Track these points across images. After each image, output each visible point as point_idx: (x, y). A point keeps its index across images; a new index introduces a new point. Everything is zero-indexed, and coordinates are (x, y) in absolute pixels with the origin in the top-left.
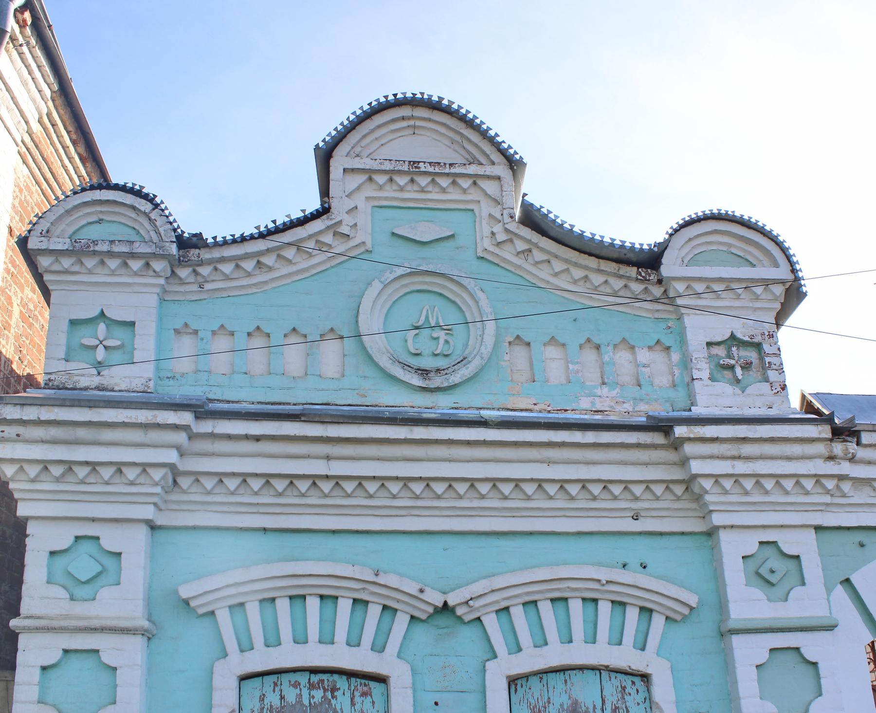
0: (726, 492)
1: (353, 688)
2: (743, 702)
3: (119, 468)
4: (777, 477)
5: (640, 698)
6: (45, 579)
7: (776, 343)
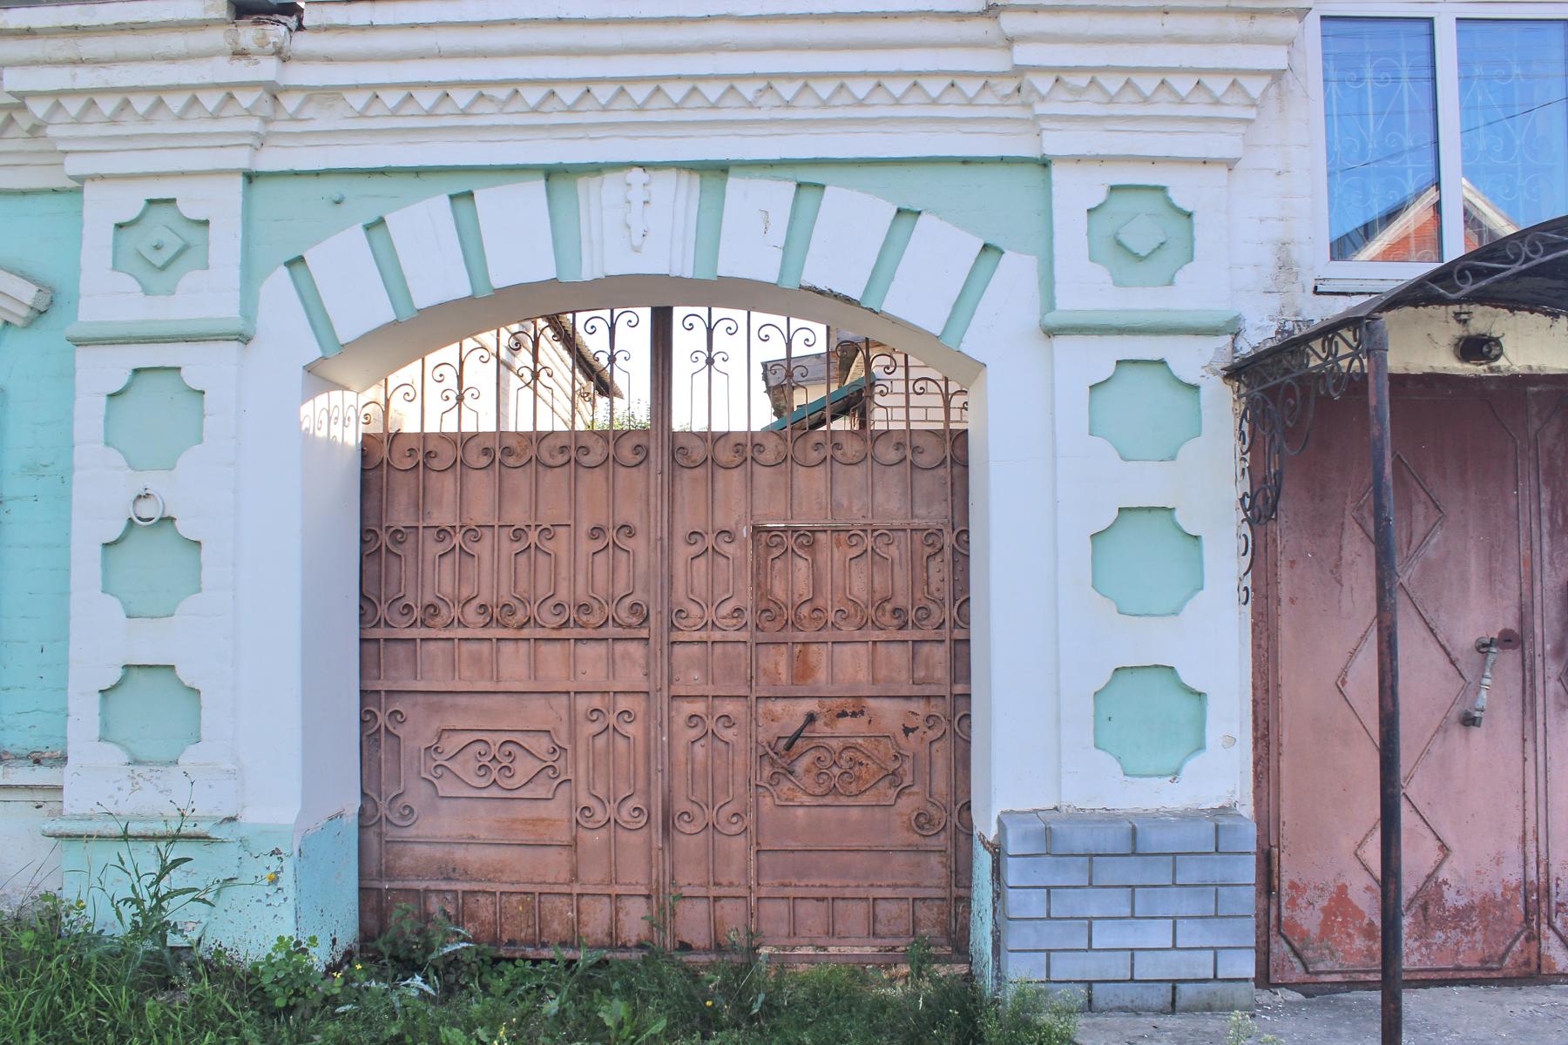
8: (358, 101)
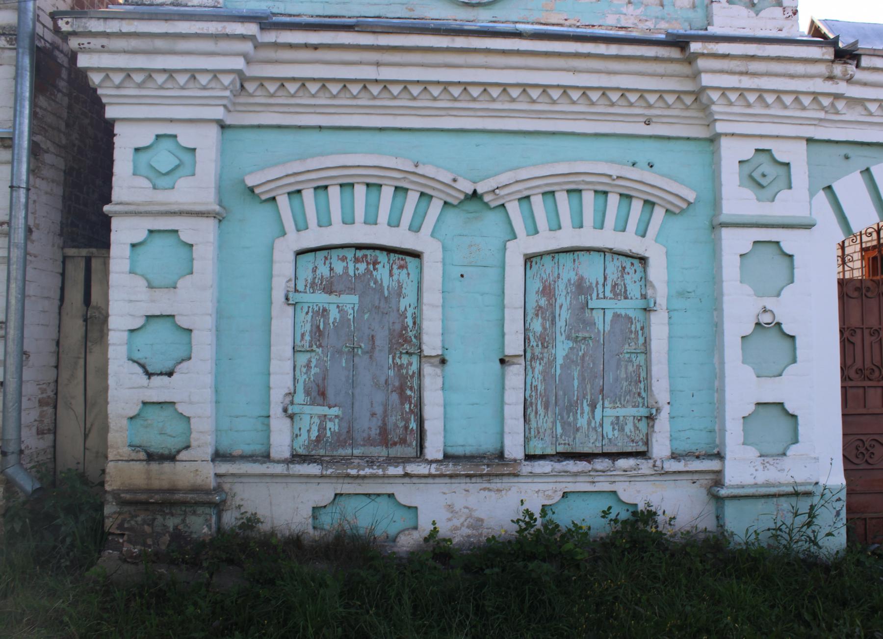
0: (731, 104)
1: (391, 262)
2: (725, 284)
3: (193, 74)
4: (778, 92)
5: (637, 277)
6: (131, 171)
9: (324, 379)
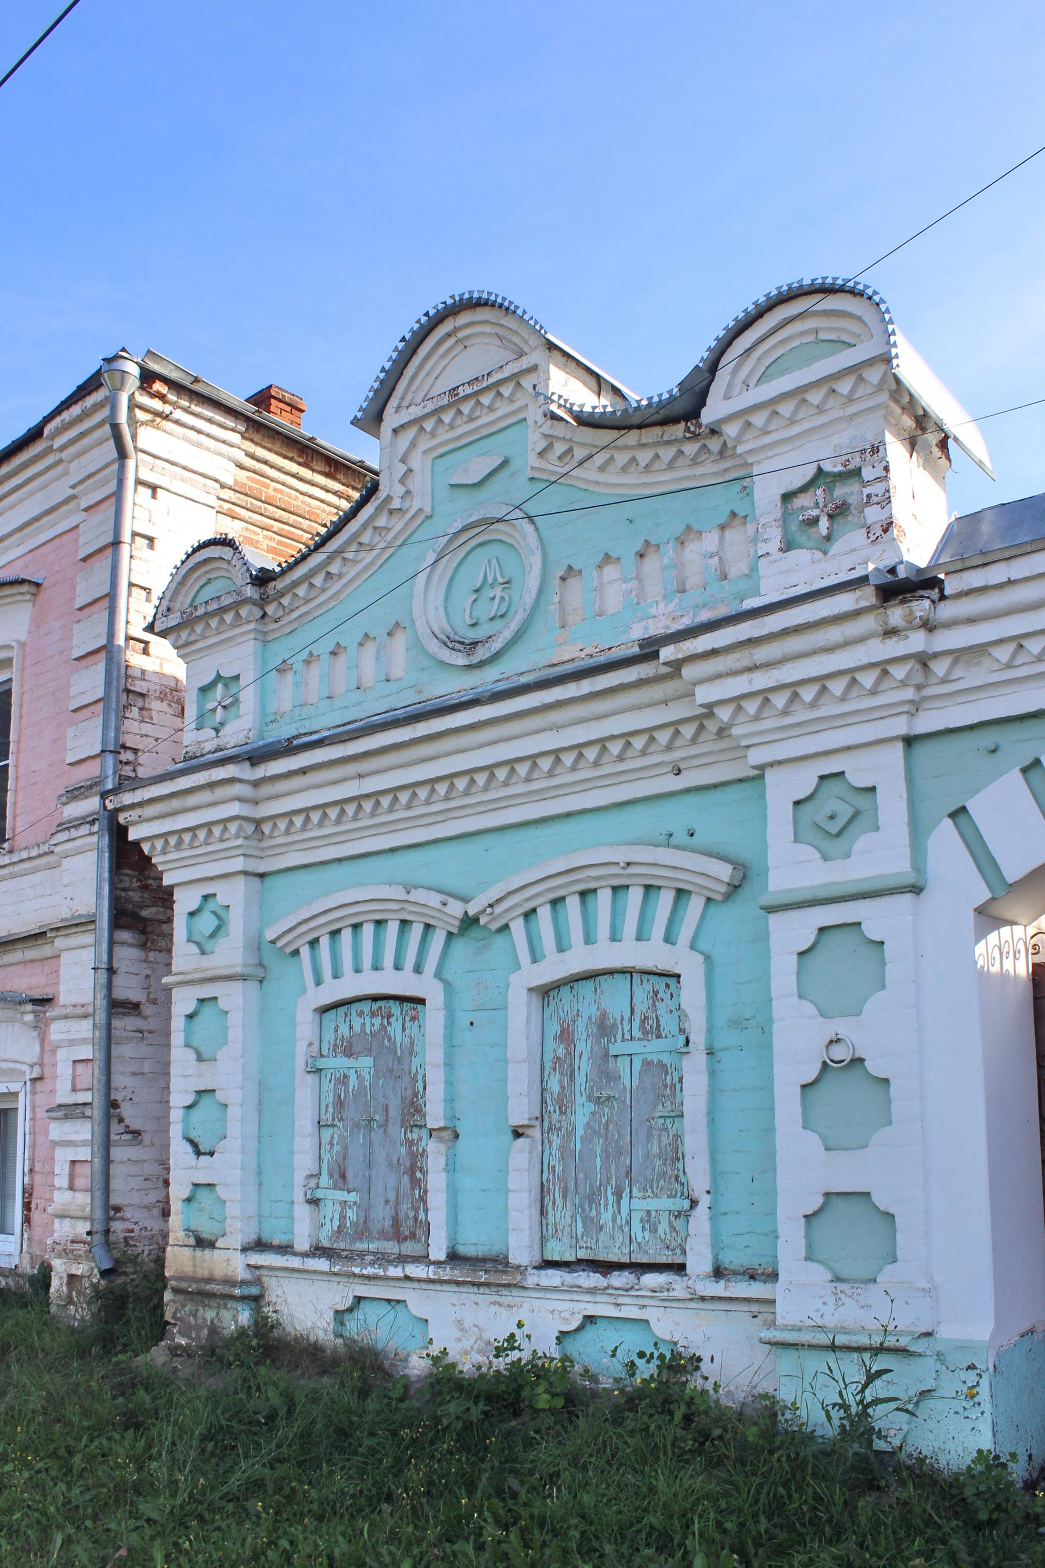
7: (883, 459)
8: (1003, 654)
9: (344, 1158)
